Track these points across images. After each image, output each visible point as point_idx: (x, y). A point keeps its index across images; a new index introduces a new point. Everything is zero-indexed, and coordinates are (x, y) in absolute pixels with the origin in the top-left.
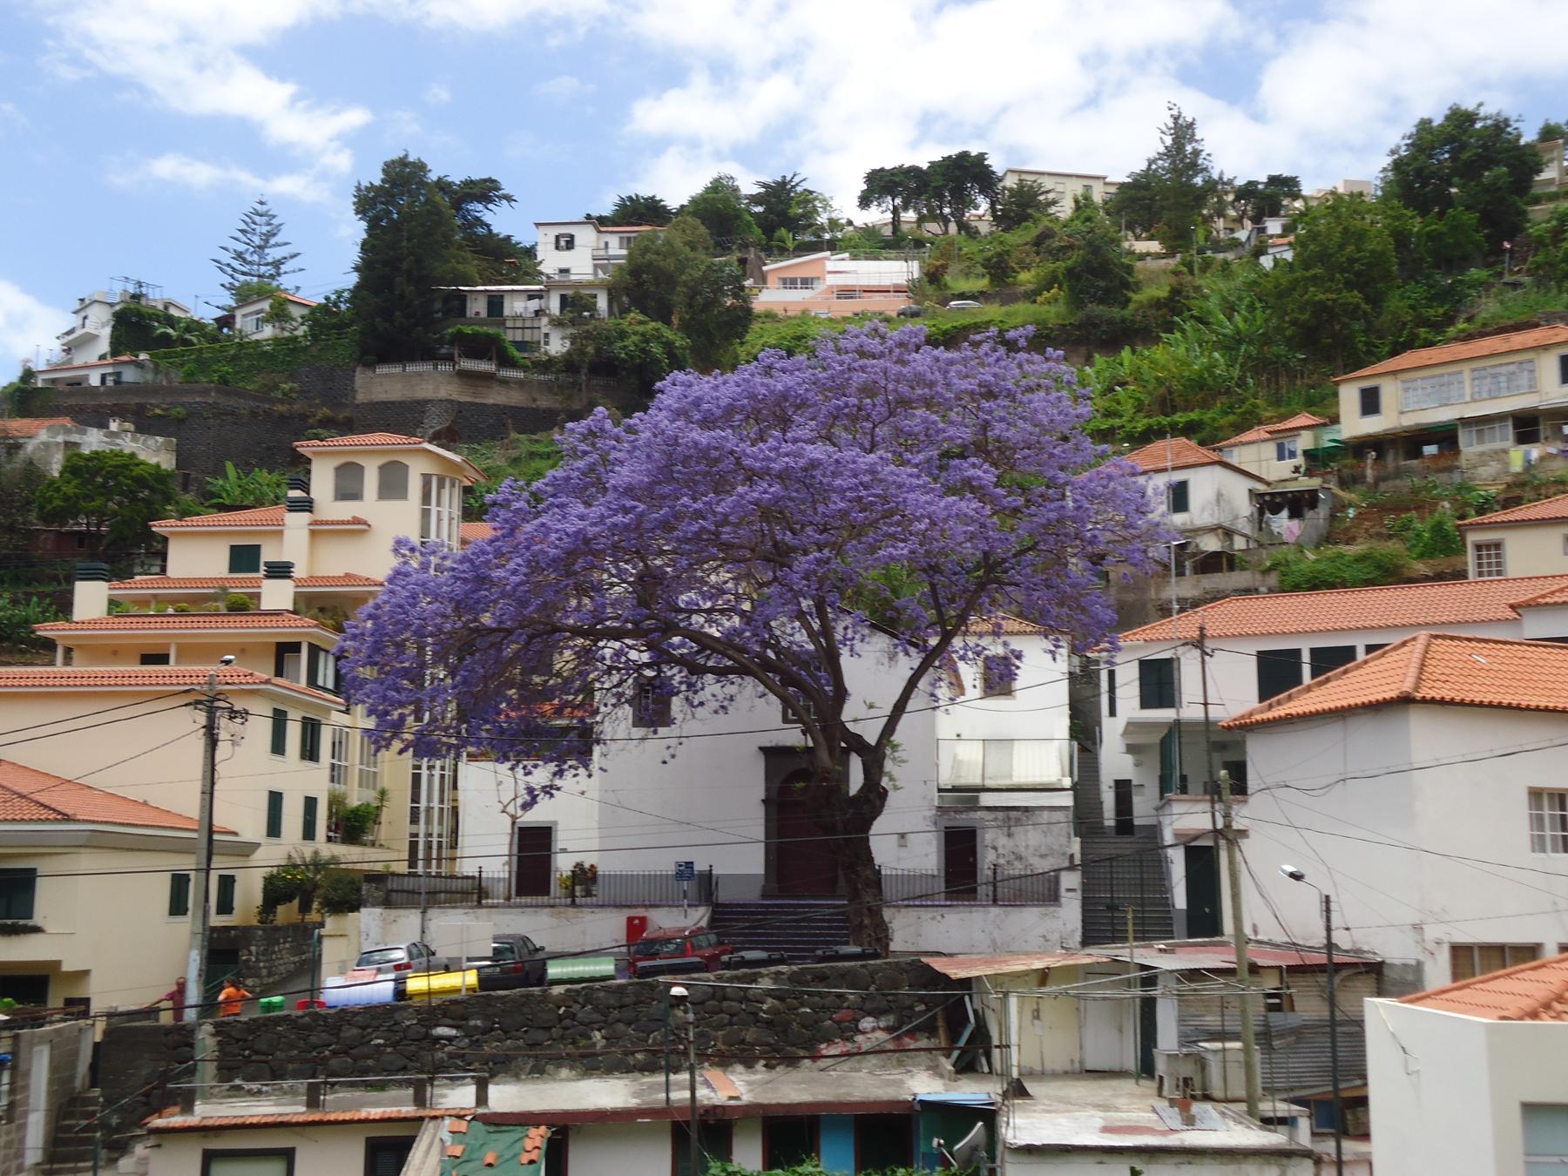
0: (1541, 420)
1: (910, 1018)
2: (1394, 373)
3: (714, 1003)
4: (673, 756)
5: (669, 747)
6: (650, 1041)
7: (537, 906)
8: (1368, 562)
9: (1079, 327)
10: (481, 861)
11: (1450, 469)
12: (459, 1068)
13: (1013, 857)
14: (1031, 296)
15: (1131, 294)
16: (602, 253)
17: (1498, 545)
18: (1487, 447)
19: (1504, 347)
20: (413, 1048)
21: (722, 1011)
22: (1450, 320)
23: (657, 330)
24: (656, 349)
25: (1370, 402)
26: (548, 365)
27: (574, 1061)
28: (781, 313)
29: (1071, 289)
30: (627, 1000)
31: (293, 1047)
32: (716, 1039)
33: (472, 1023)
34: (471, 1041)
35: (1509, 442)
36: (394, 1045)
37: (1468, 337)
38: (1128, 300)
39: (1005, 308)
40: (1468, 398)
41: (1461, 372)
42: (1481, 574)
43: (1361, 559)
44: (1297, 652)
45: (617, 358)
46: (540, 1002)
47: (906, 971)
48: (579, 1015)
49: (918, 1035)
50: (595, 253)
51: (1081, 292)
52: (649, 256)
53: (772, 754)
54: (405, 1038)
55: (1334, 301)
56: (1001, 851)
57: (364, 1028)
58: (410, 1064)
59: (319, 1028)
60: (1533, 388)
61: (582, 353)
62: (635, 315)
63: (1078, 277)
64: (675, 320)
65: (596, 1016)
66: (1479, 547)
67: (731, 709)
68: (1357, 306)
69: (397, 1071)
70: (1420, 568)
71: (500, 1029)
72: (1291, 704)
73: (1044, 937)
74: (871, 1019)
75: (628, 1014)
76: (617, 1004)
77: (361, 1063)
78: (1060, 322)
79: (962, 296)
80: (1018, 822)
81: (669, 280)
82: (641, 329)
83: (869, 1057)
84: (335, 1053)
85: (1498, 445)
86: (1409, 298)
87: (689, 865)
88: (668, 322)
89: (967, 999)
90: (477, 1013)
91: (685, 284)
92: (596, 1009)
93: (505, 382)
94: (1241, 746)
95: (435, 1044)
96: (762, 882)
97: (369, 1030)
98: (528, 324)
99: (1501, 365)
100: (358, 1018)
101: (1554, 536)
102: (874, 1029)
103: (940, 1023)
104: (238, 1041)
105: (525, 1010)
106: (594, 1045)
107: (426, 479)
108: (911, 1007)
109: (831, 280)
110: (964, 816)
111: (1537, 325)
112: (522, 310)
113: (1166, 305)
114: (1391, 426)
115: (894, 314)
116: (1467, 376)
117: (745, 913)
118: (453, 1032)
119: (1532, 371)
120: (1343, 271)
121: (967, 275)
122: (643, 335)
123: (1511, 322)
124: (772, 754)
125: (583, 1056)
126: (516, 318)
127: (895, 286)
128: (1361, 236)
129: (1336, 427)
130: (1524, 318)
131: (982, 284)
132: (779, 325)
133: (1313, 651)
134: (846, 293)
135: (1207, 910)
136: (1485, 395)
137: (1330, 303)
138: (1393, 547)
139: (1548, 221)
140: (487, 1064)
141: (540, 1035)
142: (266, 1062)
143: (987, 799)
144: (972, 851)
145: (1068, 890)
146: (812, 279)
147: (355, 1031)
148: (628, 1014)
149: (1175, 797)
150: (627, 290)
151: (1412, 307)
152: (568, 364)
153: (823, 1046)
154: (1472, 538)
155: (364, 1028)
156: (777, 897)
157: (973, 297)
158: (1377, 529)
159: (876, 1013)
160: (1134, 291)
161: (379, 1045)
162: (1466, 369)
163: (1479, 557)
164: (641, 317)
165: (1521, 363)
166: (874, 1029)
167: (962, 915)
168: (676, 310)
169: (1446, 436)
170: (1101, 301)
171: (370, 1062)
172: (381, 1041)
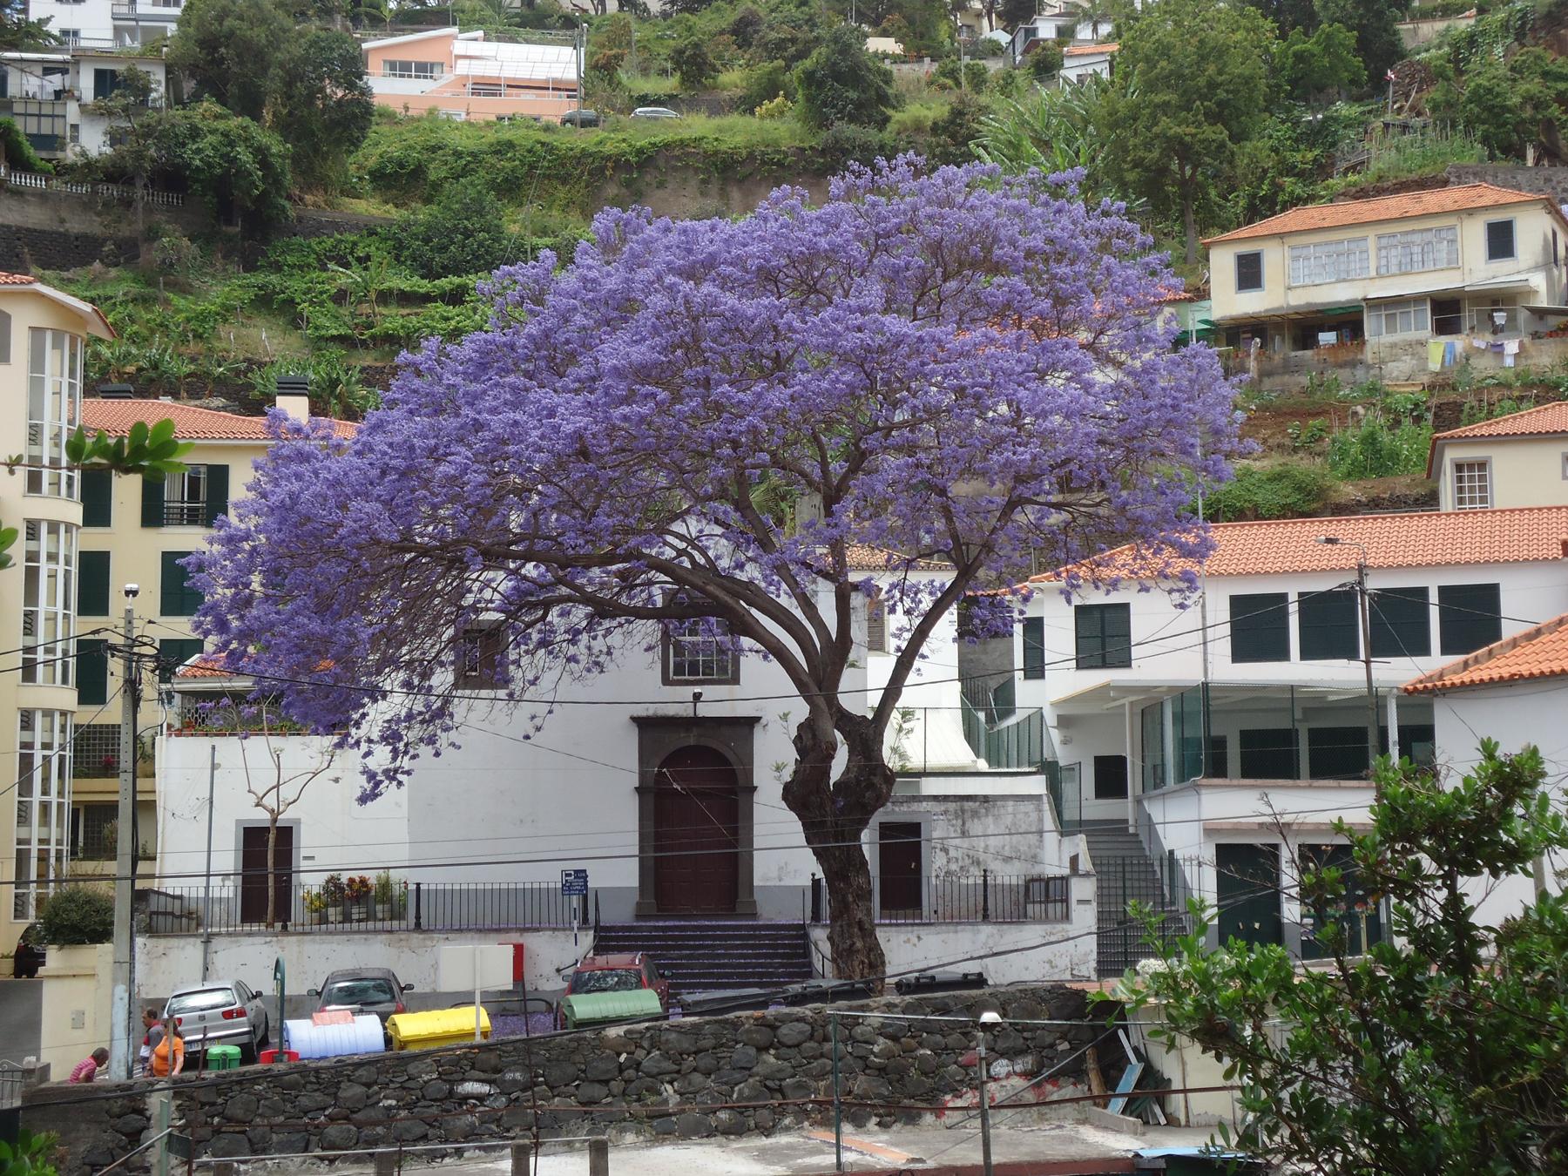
0: (1466, 305)
1: (1051, 1059)
2: (1281, 236)
3: (812, 1044)
4: (538, 729)
5: (533, 718)
6: (735, 1096)
7: (367, 932)
8: (1286, 482)
9: (823, 153)
10: (1340, 813)
11: (1353, 364)
12: (492, 1135)
13: (968, 862)
14: (747, 104)
15: (890, 112)
16: (124, 10)
17: (1482, 465)
18: (1399, 337)
19: (1416, 209)
20: (434, 1110)
21: (822, 1055)
22: (1323, 169)
23: (245, 129)
24: (244, 155)
25: (1249, 273)
26: (88, 170)
27: (640, 1123)
28: (400, 110)
29: (809, 99)
30: (708, 1042)
31: (277, 1112)
32: (817, 1091)
33: (509, 1076)
34: (510, 1101)
35: (1427, 332)
36: (410, 1106)
37: (1361, 194)
38: (887, 119)
39: (716, 121)
40: (1373, 273)
41: (1365, 239)
42: (1461, 501)
43: (1277, 478)
44: (1423, 592)
45: (188, 166)
46: (594, 1048)
47: (1044, 1000)
48: (645, 1063)
49: (1062, 1081)
50: (117, 10)
51: (825, 104)
52: (229, 22)
53: (647, 726)
54: (424, 1097)
55: (1194, 136)
56: (952, 853)
57: (369, 1085)
58: (431, 1132)
59: (309, 1087)
60: (1453, 264)
61: (139, 156)
62: (208, 105)
63: (820, 85)
64: (267, 115)
65: (668, 1065)
66: (1459, 467)
67: (610, 667)
68: (1222, 145)
69: (416, 1141)
70: (1349, 491)
71: (546, 1083)
72: (1492, 663)
73: (1050, 962)
74: (1005, 1062)
75: (706, 1061)
76: (693, 1049)
77: (366, 1131)
78: (797, 143)
79: (644, 100)
80: (975, 814)
81: (258, 57)
82: (221, 125)
83: (1004, 1111)
84: (331, 1119)
85: (1412, 335)
86: (1270, 137)
87: (581, 875)
88: (256, 117)
89: (1121, 1033)
90: (515, 1063)
91: (282, 65)
92: (666, 1056)
93: (18, 193)
94: (1429, 709)
95: (460, 1105)
96: (637, 898)
97: (376, 1088)
98: (46, 110)
99: (1414, 232)
100: (360, 1072)
101: (1551, 455)
102: (1008, 1076)
103: (1091, 1064)
104: (203, 1105)
105: (578, 1058)
106: (666, 1101)
107: (36, 332)
108: (1052, 1046)
109: (462, 68)
110: (905, 808)
111: (1445, 183)
112: (36, 89)
113: (945, 129)
114: (1276, 304)
115: (558, 121)
116: (1372, 243)
117: (636, 938)
118: (486, 1089)
119: (1452, 241)
120: (1203, 98)
121: (645, 72)
122: (225, 135)
123: (1414, 176)
124: (647, 726)
125: (651, 1117)
126: (27, 99)
127: (555, 81)
128: (1221, 52)
129: (1204, 304)
130: (1428, 171)
131: (671, 84)
132: (399, 129)
133: (1442, 590)
134: (486, 87)
135: (1257, 925)
136: (1394, 269)
137: (1188, 139)
138: (1303, 465)
139: (1439, 47)
140: (530, 1129)
141: (597, 1091)
142: (244, 1132)
143: (930, 787)
144: (915, 852)
145: (1080, 902)
146: (432, 65)
147: (359, 1090)
148: (706, 1061)
149: (1205, 781)
150: (193, 70)
151: (1275, 150)
152: (113, 173)
153: (948, 1097)
154: (1451, 455)
155: (369, 1085)
156: (658, 918)
157: (658, 102)
158: (1278, 439)
159: (1011, 1054)
160: (894, 108)
161: (389, 1108)
162: (1371, 234)
163: (1460, 479)
164: (218, 109)
165: (1439, 230)
166: (1008, 1076)
167: (944, 936)
168: (269, 101)
169: (1348, 321)
170: (852, 119)
171: (380, 1130)
172: (394, 1102)
